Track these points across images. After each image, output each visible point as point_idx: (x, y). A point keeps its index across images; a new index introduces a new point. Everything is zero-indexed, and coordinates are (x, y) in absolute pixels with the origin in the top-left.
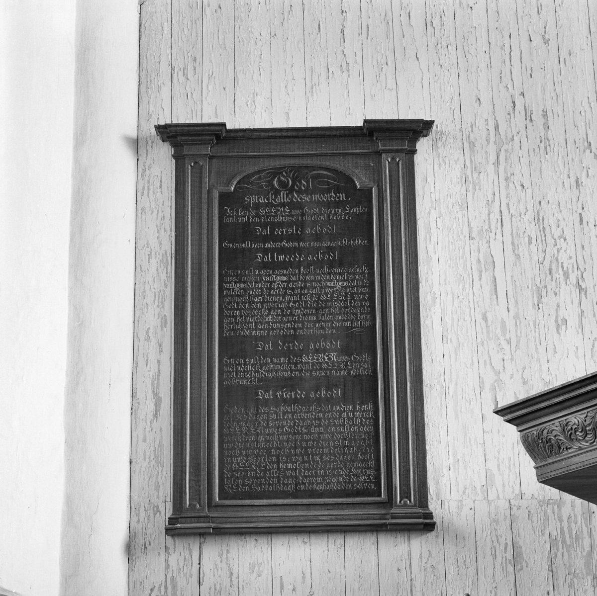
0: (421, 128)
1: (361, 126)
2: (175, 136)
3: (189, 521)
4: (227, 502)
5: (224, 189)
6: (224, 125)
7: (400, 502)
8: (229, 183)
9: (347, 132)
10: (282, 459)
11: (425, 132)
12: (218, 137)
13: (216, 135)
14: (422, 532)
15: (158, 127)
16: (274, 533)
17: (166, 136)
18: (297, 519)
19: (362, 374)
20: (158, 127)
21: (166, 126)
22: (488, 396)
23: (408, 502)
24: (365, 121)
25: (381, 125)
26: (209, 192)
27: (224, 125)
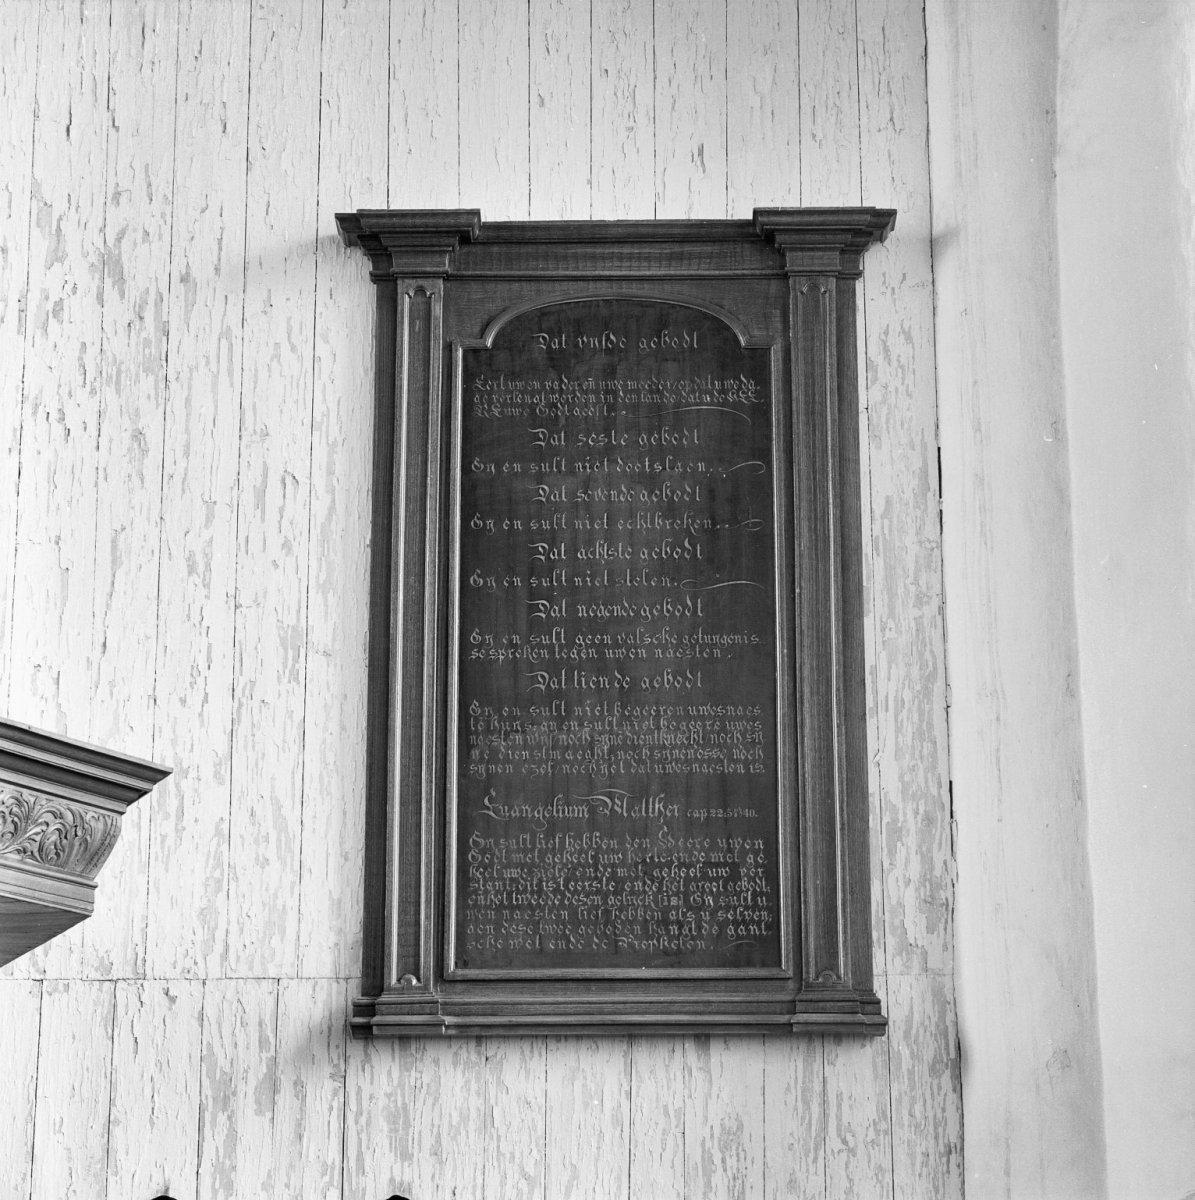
0: (872, 225)
1: (749, 220)
2: (375, 237)
3: (778, 1010)
4: (472, 973)
5: (475, 343)
6: (476, 213)
7: (399, 980)
8: (482, 334)
9: (731, 231)
10: (547, 887)
11: (877, 233)
12: (465, 239)
13: (454, 233)
14: (817, 1044)
15: (342, 219)
16: (733, 1036)
17: (356, 235)
18: (406, 1010)
19: (704, 715)
20: (342, 219)
21: (362, 215)
22: (187, 785)
23: (414, 982)
24: (756, 212)
25: (643, 230)
26: (449, 349)
27: (476, 213)
